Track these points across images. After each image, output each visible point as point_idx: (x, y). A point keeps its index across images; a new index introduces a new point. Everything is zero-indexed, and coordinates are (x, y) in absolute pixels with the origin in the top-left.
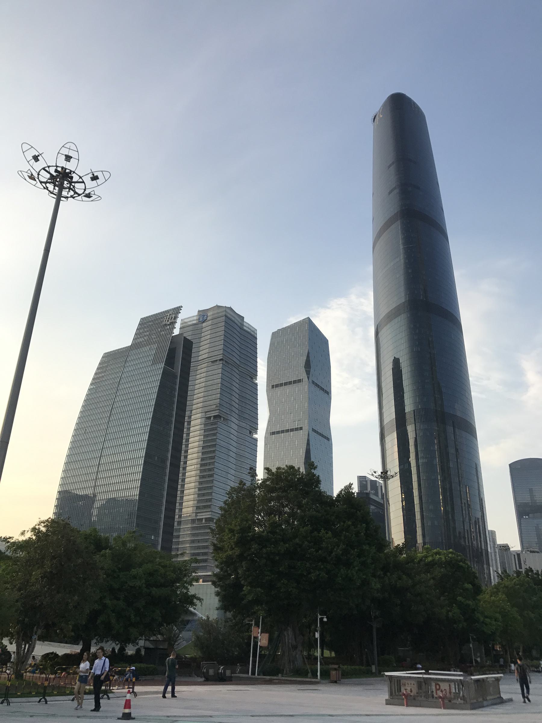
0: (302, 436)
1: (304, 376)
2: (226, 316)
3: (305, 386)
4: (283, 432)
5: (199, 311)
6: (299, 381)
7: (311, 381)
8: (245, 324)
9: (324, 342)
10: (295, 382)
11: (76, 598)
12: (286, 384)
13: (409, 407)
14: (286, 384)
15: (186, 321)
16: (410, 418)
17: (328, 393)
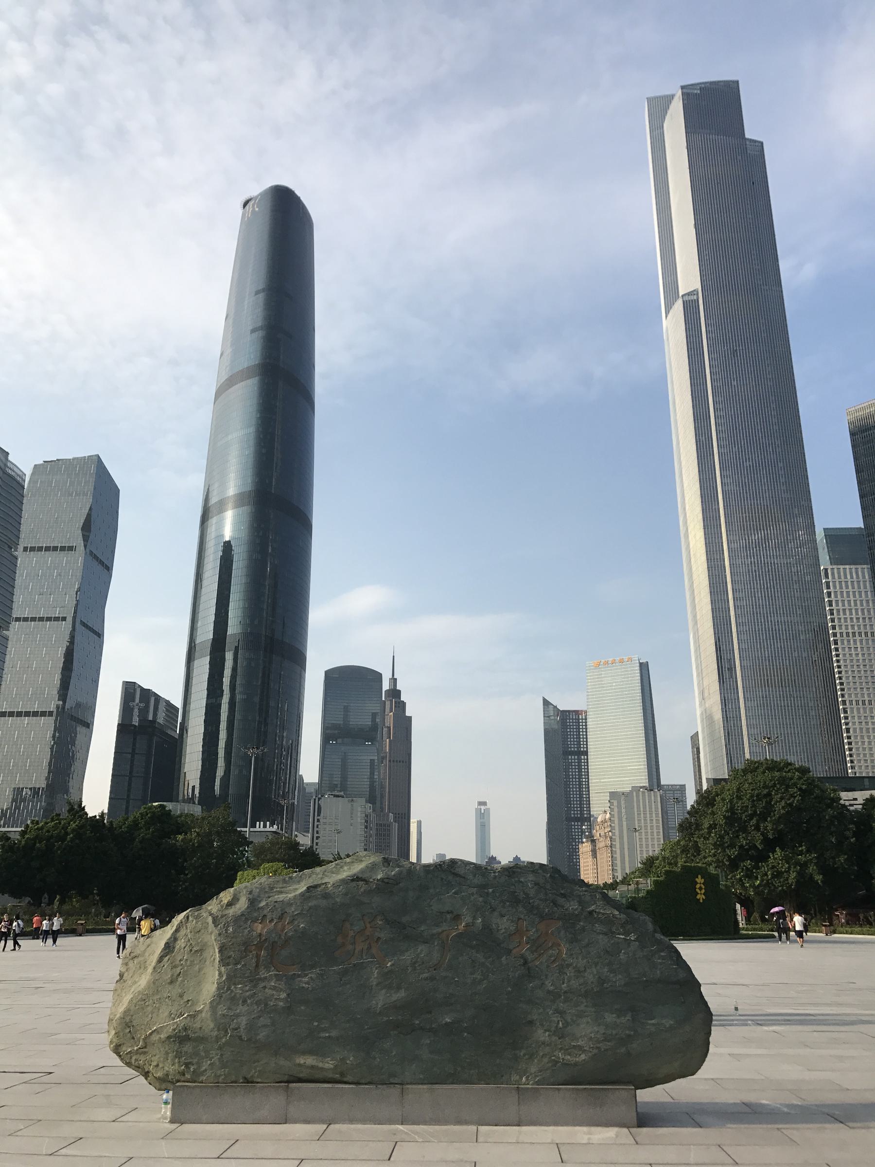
0: (65, 627)
1: (79, 542)
3: (78, 558)
4: (33, 619)
6: (71, 548)
7: (88, 550)
8: (9, 464)
9: (114, 492)
10: (63, 549)
12: (48, 549)
13: (234, 627)
14: (48, 549)
16: (230, 644)
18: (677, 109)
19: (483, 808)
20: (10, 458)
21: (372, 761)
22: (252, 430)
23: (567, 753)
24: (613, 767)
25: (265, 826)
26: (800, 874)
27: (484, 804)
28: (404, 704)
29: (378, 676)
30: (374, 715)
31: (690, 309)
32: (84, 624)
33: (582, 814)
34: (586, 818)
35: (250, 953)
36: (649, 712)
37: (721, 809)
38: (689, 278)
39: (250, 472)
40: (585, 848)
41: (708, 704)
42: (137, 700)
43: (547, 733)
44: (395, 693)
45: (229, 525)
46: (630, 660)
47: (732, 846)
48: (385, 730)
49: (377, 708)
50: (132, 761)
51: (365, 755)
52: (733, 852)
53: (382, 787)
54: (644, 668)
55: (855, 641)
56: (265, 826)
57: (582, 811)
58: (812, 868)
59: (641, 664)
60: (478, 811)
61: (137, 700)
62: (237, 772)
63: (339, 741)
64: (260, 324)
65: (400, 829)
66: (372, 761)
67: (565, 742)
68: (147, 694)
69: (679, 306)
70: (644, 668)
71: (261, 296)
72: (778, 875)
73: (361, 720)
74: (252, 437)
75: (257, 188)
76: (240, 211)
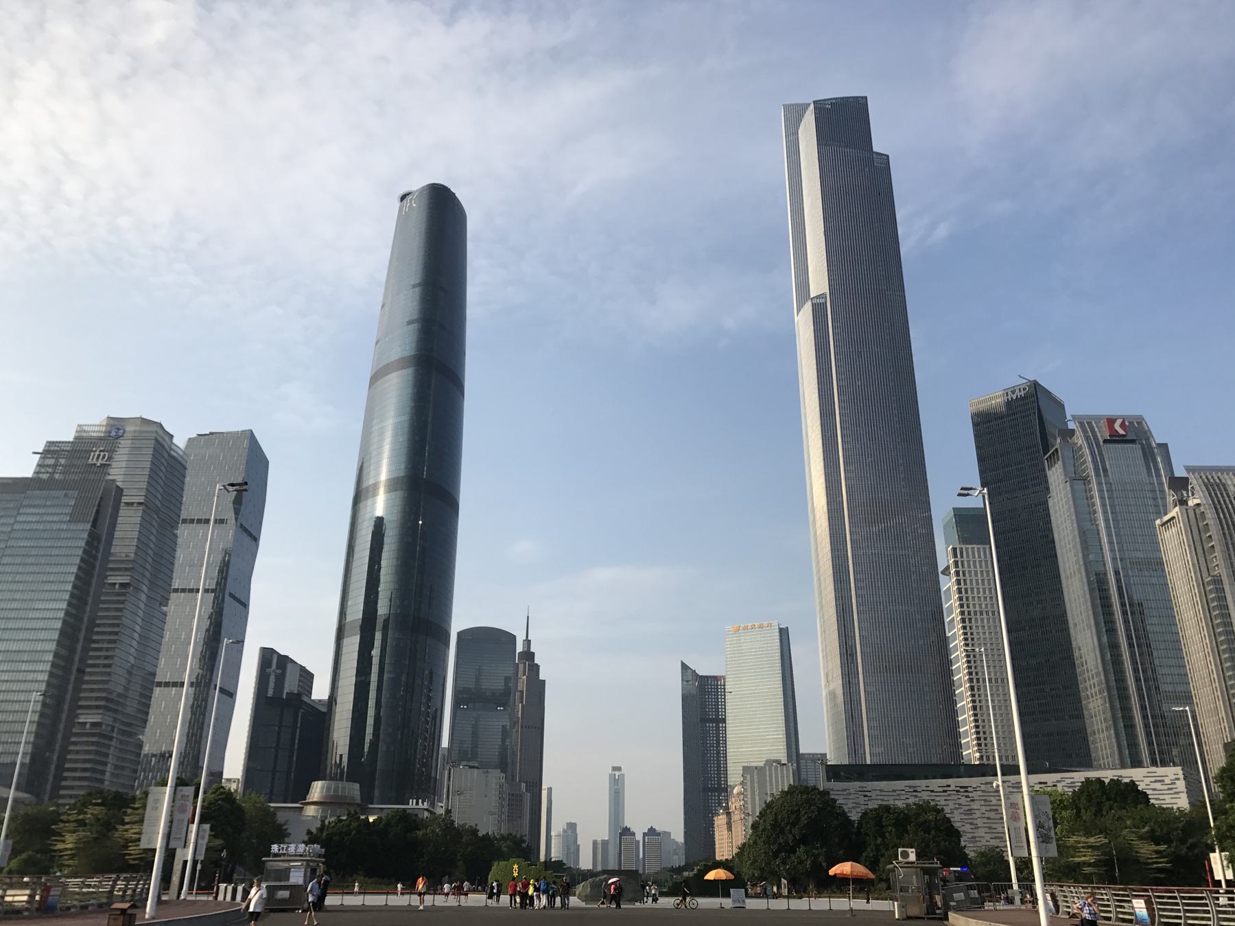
2: (156, 440)
5: (109, 418)
9: (265, 463)
11: (1128, 822)
13: (383, 609)
15: (86, 428)
17: (256, 539)
18: (809, 119)
19: (617, 773)
20: (175, 441)
21: (504, 727)
22: (406, 418)
23: (705, 720)
24: (752, 740)
25: (417, 803)
26: (813, 862)
27: (619, 769)
28: (537, 666)
29: (512, 638)
30: (507, 679)
32: (232, 595)
33: (719, 784)
34: (722, 789)
35: (593, 886)
36: (789, 682)
37: (770, 818)
38: (819, 283)
39: (403, 459)
40: (720, 820)
41: (832, 687)
42: (274, 666)
43: (685, 698)
44: (528, 655)
45: (380, 505)
46: (770, 625)
47: (775, 843)
48: (518, 694)
49: (509, 672)
50: (279, 734)
51: (495, 722)
52: (775, 847)
53: (514, 754)
54: (784, 634)
55: (982, 620)
56: (417, 803)
57: (719, 780)
58: (821, 858)
59: (781, 630)
60: (612, 777)
61: (274, 666)
62: (384, 748)
63: (471, 705)
64: (416, 317)
65: (532, 800)
66: (504, 727)
67: (703, 705)
68: (284, 661)
69: (808, 307)
70: (784, 634)
71: (417, 290)
72: (801, 862)
73: (493, 683)
74: (406, 425)
75: (418, 182)
76: (398, 204)
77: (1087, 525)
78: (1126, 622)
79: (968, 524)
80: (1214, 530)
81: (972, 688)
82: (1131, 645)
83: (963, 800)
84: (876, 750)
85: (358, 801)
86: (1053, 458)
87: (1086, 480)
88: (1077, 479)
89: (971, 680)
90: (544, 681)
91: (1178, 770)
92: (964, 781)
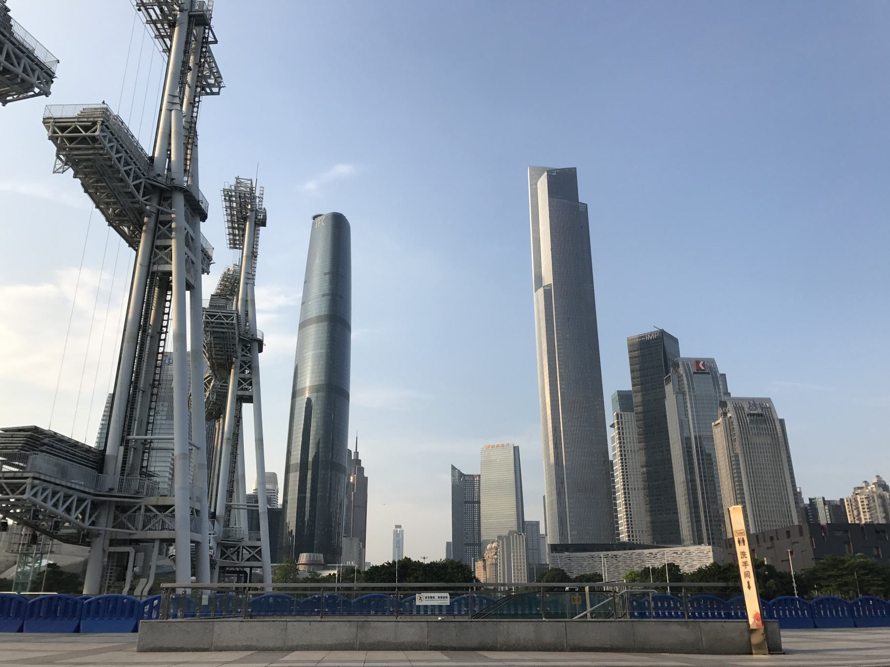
24: (496, 515)
27: (400, 527)
31: (547, 293)
38: (548, 278)
59: (514, 447)
60: (395, 532)
67: (465, 494)
69: (541, 291)
75: (327, 210)
77: (683, 417)
78: (699, 468)
79: (624, 398)
80: (737, 430)
81: (625, 493)
82: (701, 481)
83: (615, 562)
84: (574, 533)
85: (323, 562)
86: (668, 380)
87: (684, 394)
88: (680, 392)
89: (624, 489)
90: (367, 478)
91: (710, 547)
92: (615, 553)
